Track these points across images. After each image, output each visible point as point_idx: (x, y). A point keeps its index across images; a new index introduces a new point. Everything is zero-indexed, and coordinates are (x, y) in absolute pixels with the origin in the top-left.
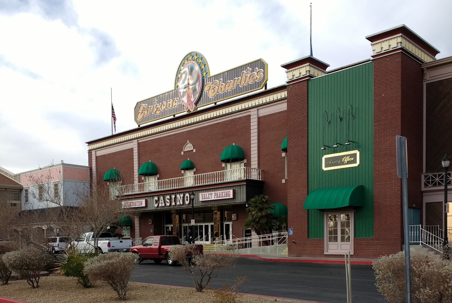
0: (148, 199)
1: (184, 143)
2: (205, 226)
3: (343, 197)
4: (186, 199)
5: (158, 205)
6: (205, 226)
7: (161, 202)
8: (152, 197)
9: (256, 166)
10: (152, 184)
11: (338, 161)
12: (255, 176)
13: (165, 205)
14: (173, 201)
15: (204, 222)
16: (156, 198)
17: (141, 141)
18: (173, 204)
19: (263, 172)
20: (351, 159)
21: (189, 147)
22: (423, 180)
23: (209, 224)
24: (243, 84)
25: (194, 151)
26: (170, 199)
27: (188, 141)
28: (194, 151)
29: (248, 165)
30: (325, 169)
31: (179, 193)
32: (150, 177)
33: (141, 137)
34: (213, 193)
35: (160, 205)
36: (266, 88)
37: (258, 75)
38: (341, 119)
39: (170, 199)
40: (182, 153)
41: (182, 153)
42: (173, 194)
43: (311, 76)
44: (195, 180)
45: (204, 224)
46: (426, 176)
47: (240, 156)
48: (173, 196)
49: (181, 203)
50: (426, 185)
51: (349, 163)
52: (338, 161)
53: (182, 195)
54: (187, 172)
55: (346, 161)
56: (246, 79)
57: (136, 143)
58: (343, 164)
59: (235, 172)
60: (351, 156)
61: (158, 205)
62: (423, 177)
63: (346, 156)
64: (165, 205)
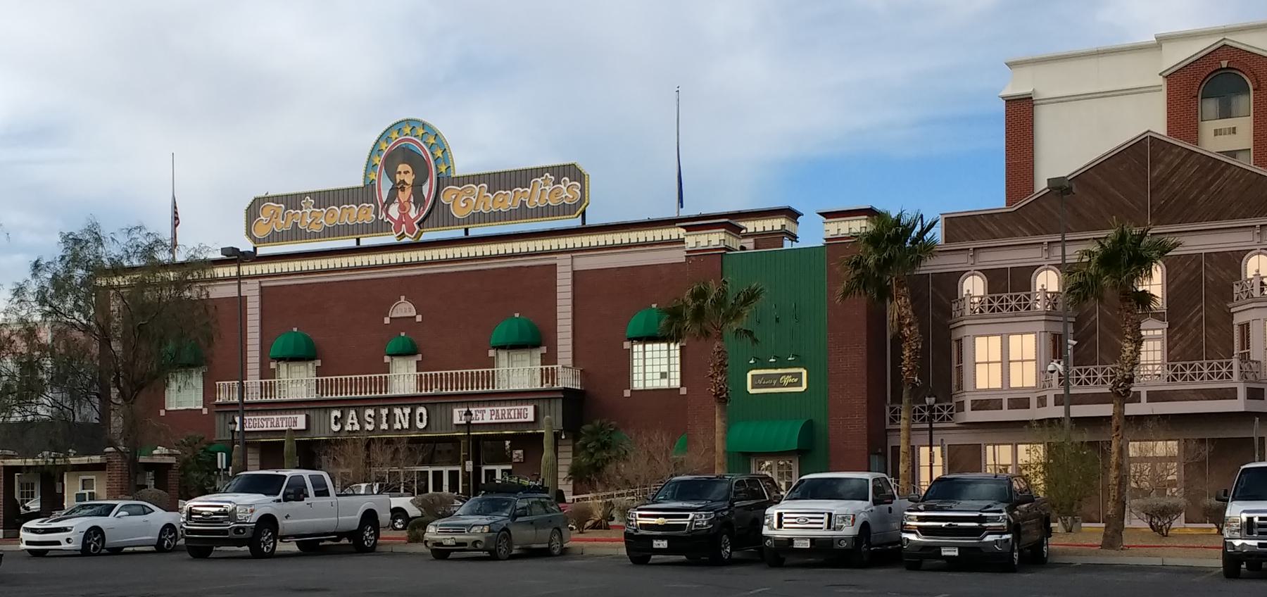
0: (312, 413)
1: (394, 300)
2: (450, 472)
3: (788, 434)
4: (418, 418)
5: (342, 428)
6: (450, 472)
7: (350, 421)
8: (322, 413)
9: (569, 362)
10: (298, 382)
11: (776, 380)
12: (567, 379)
13: (362, 428)
14: (384, 419)
15: (431, 464)
16: (337, 413)
17: (268, 283)
18: (384, 426)
19: (585, 375)
20: (795, 381)
21: (404, 309)
22: (888, 414)
23: (446, 470)
24: (535, 202)
25: (419, 318)
26: (377, 418)
27: (403, 298)
28: (419, 318)
29: (550, 358)
30: (751, 391)
31: (401, 406)
32: (290, 364)
33: (269, 276)
34: (488, 409)
35: (348, 428)
36: (584, 222)
37: (568, 191)
38: (777, 320)
39: (377, 418)
40: (387, 320)
41: (387, 320)
42: (384, 406)
43: (728, 249)
44: (420, 380)
45: (430, 470)
46: (891, 409)
47: (535, 339)
48: (384, 412)
49: (406, 426)
50: (892, 422)
51: (790, 385)
52: (776, 380)
53: (407, 411)
54: (395, 359)
55: (786, 382)
56: (541, 193)
57: (257, 286)
58: (782, 385)
59: (519, 372)
60: (794, 375)
61: (342, 428)
62: (887, 408)
63: (787, 374)
64: (362, 428)
